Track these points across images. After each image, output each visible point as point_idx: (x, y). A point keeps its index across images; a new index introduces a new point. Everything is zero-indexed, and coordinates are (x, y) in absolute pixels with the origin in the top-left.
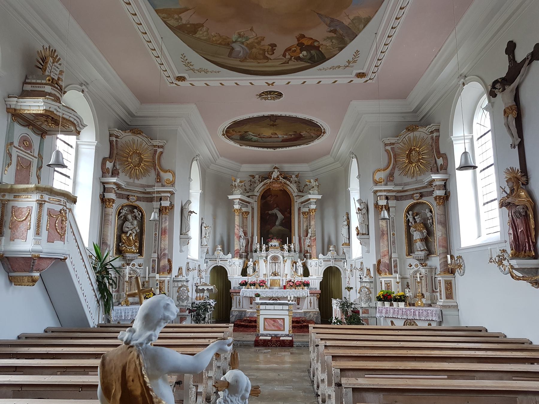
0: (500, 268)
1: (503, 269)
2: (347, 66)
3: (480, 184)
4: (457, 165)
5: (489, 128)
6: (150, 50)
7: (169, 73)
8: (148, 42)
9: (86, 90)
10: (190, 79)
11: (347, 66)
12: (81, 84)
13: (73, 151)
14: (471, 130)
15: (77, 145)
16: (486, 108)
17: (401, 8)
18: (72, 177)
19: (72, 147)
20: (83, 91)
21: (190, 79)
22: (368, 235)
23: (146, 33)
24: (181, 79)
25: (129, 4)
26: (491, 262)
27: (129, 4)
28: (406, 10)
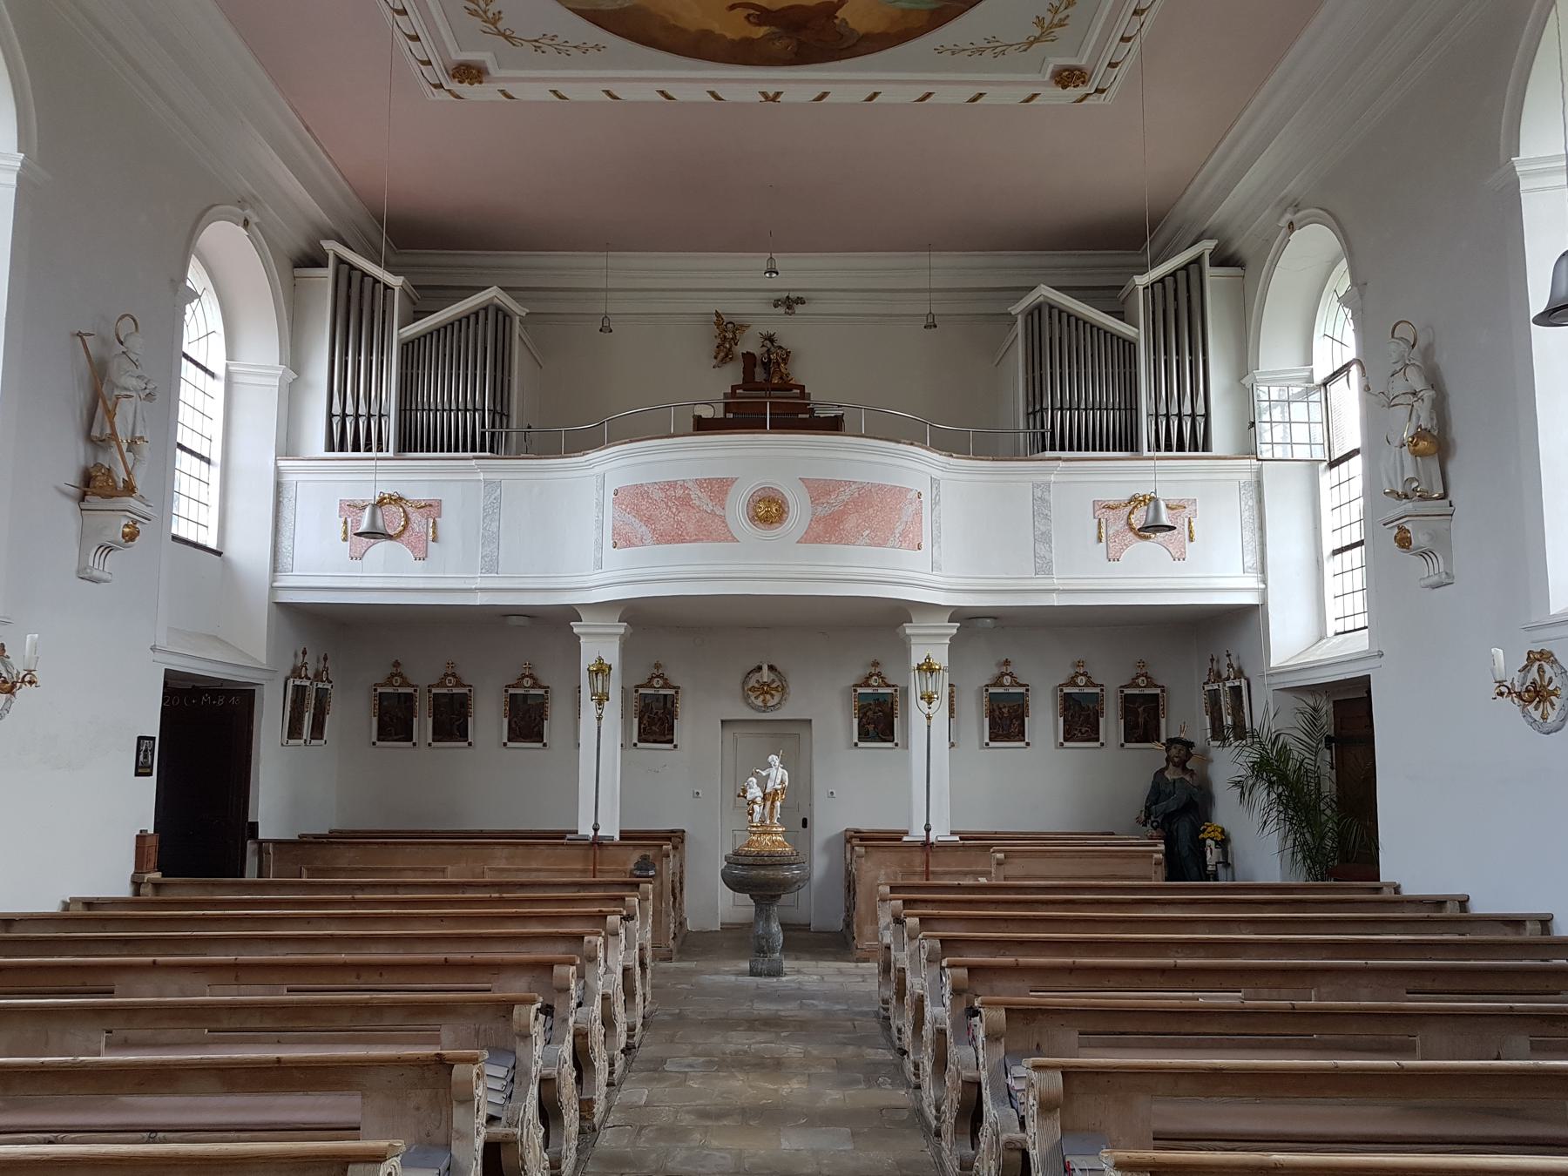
0: (1525, 714)
1: (1537, 715)
2: (1037, 40)
3: (1326, 501)
4: (1538, 302)
5: (1351, 353)
6: (389, 12)
7: (426, 48)
8: (423, 63)
9: (254, 219)
10: (503, 73)
11: (1037, 40)
12: (241, 203)
13: (217, 388)
14: (1308, 360)
15: (229, 374)
16: (1344, 301)
17: (1123, 39)
18: (216, 457)
19: (213, 375)
20: (246, 224)
21: (503, 73)
22: (1444, 496)
23: (429, 63)
24: (469, 73)
25: (404, 12)
26: (1501, 694)
27: (404, 12)
28: (1149, 18)
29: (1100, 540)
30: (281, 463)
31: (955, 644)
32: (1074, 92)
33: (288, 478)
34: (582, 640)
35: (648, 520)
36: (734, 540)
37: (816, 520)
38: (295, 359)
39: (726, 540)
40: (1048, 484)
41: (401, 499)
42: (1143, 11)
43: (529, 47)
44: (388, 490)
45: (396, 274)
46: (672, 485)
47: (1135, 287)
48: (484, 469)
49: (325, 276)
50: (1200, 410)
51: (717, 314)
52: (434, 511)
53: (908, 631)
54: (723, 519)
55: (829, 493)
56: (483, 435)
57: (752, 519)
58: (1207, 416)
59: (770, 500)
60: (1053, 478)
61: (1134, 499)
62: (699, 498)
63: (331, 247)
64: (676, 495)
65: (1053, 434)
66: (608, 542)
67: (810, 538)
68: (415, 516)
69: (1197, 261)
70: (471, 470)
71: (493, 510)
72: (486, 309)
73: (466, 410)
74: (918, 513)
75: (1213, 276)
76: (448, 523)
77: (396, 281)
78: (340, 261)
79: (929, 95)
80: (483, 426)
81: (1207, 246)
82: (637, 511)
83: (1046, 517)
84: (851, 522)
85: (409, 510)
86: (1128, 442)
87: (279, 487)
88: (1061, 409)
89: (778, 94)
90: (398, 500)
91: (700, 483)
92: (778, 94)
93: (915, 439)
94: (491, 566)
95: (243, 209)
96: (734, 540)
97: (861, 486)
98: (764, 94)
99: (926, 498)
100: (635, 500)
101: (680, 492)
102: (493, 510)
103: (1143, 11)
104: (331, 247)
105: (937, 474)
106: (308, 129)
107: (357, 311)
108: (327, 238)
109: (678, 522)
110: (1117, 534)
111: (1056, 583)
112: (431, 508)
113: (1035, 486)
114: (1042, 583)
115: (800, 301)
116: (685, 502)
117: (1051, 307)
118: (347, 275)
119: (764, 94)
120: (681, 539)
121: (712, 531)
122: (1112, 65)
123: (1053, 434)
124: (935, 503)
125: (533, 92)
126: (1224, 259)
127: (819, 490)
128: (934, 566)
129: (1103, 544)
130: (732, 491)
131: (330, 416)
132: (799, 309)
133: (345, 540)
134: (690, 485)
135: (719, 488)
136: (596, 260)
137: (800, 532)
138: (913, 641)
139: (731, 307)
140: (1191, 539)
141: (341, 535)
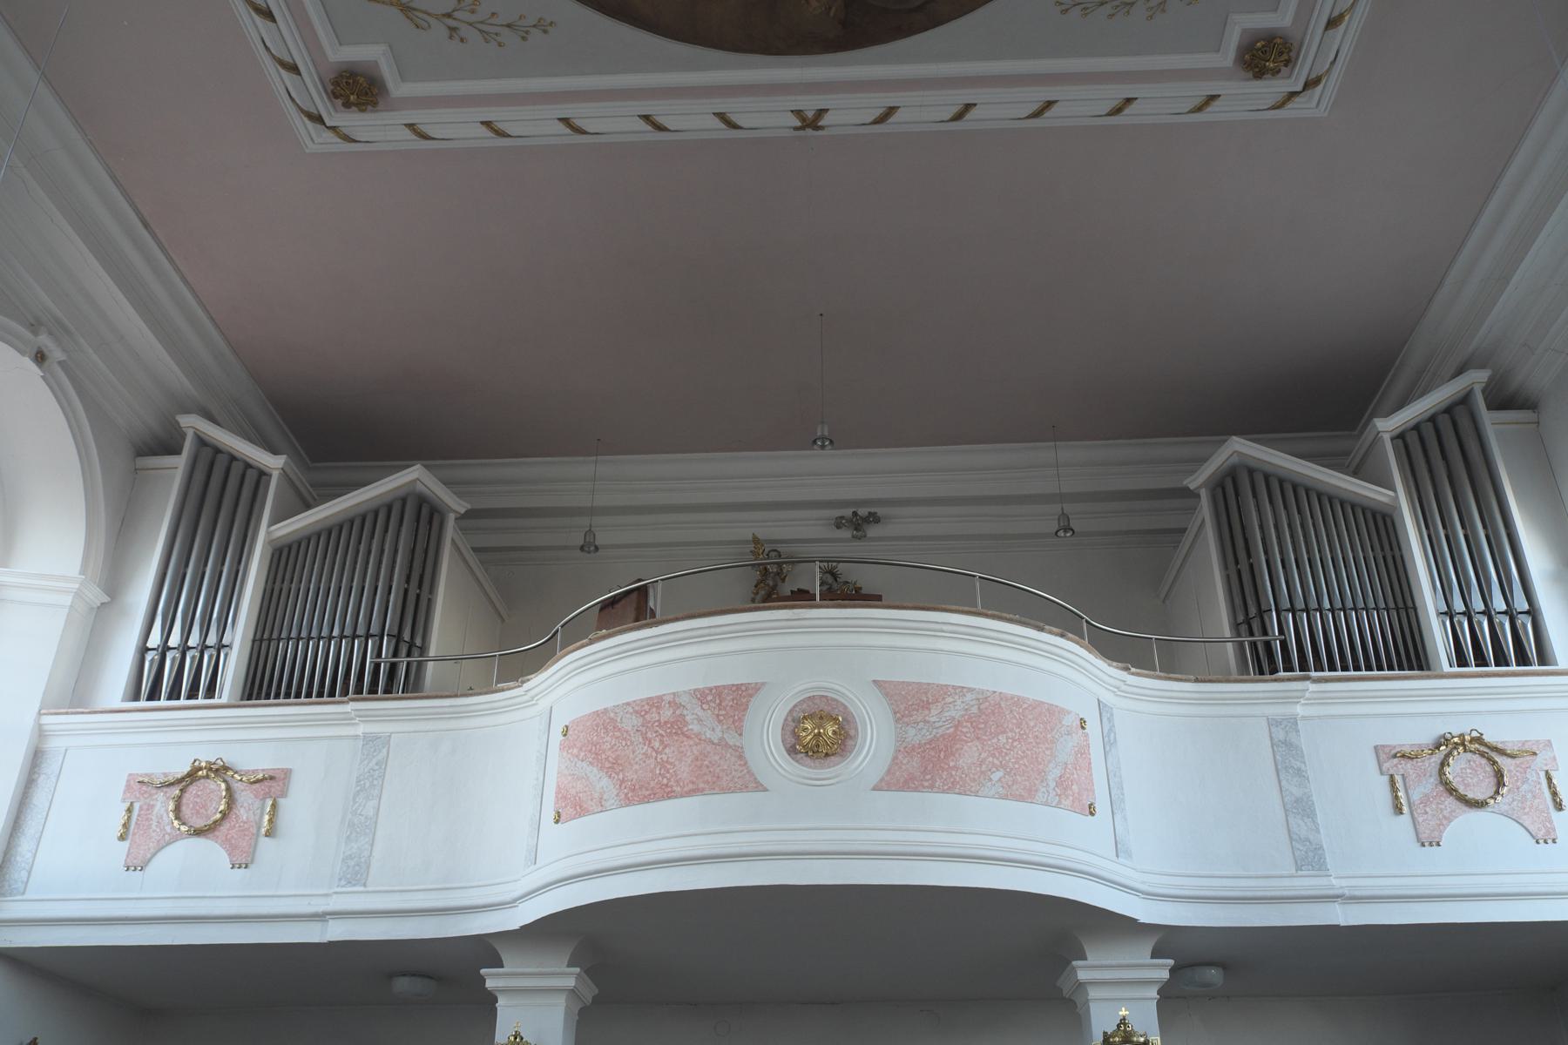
9: (56, 354)
12: (35, 326)
20: (40, 358)
24: (357, 88)
29: (1398, 810)
30: (46, 720)
31: (1171, 999)
32: (1274, 88)
33: (54, 744)
34: (502, 1002)
35: (613, 767)
36: (760, 787)
37: (904, 750)
38: (113, 582)
39: (744, 788)
40: (1293, 722)
41: (226, 768)
42: (1341, 16)
43: (439, 30)
44: (206, 756)
45: (275, 451)
46: (655, 703)
47: (1377, 438)
48: (366, 717)
49: (178, 465)
50: (1521, 604)
51: (756, 541)
52: (276, 787)
53: (1082, 975)
54: (740, 754)
55: (926, 706)
56: (377, 666)
57: (792, 751)
58: (1533, 612)
59: (821, 717)
60: (1299, 710)
61: (1442, 741)
62: (702, 723)
63: (192, 423)
64: (660, 720)
65: (1284, 644)
66: (549, 814)
67: (898, 780)
68: (245, 796)
69: (1465, 400)
70: (346, 720)
71: (370, 782)
72: (404, 500)
73: (354, 636)
74: (1083, 751)
75: (1490, 421)
76: (298, 807)
77: (273, 463)
78: (202, 442)
79: (1049, 104)
80: (379, 655)
81: (1477, 378)
82: (595, 754)
83: (1299, 772)
84: (969, 755)
85: (236, 786)
86: (1409, 655)
87: (36, 759)
88: (1293, 610)
89: (821, 112)
90: (220, 770)
91: (701, 696)
92: (821, 112)
93: (1066, 625)
94: (356, 873)
95: (35, 333)
96: (760, 787)
97: (983, 698)
98: (798, 113)
99: (1093, 727)
100: (599, 740)
101: (667, 714)
102: (370, 782)
103: (1341, 16)
104: (192, 423)
105: (1108, 698)
106: (146, 225)
107: (217, 504)
108: (187, 411)
109: (663, 764)
110: (1426, 800)
111: (1337, 884)
112: (272, 783)
113: (1272, 723)
114: (1308, 883)
115: (874, 519)
116: (676, 728)
117: (1251, 472)
118: (210, 457)
119: (798, 113)
120: (669, 795)
121: (724, 774)
122: (1332, 23)
123: (1284, 644)
124: (1109, 743)
125: (459, 129)
126: (1504, 399)
127: (909, 701)
128: (1119, 849)
129: (1405, 818)
130: (755, 703)
131: (144, 650)
132: (873, 531)
133: (122, 838)
134: (684, 700)
135: (732, 702)
136: (581, 467)
137: (875, 775)
138: (1093, 993)
139: (773, 528)
140: (1559, 806)
141: (119, 829)
